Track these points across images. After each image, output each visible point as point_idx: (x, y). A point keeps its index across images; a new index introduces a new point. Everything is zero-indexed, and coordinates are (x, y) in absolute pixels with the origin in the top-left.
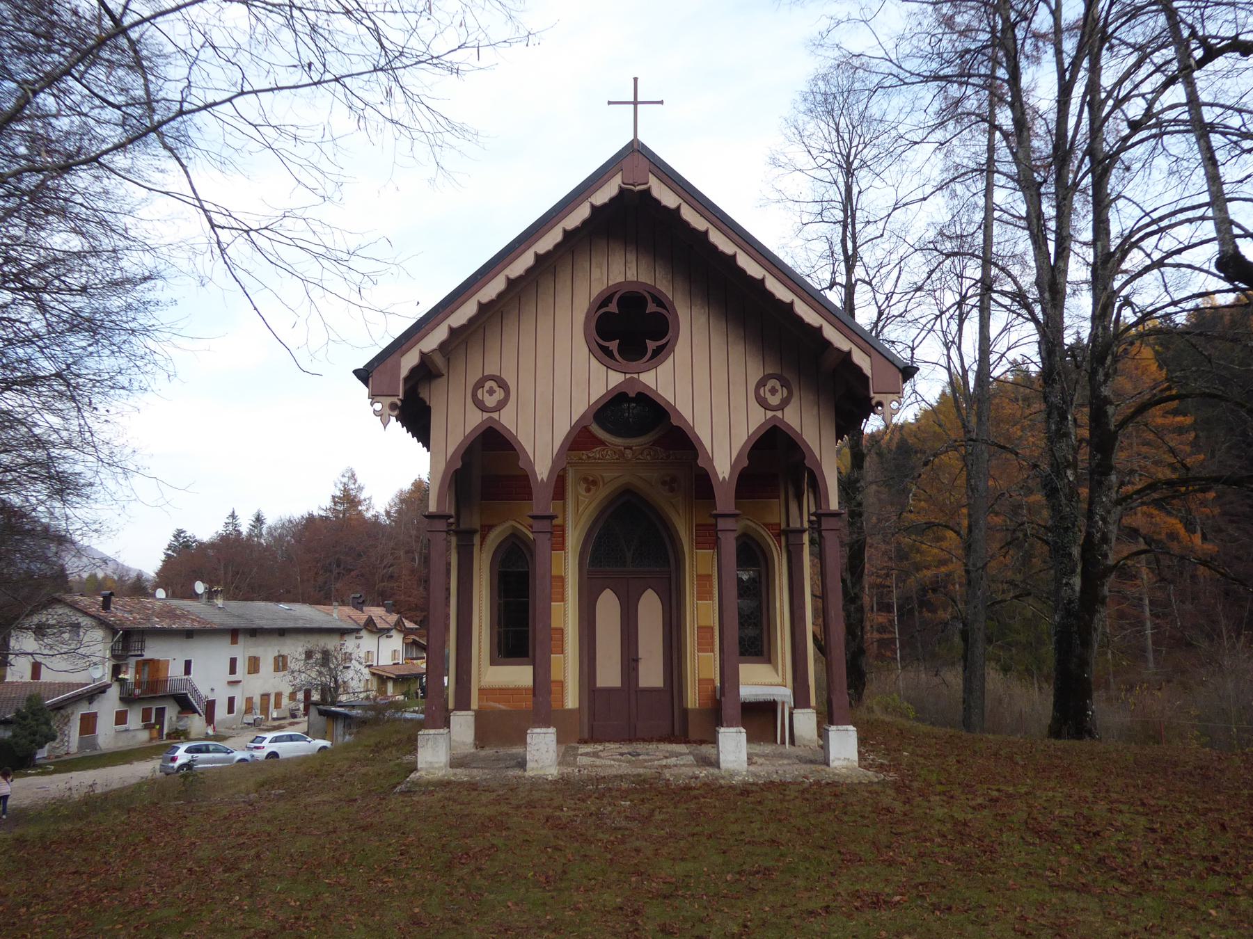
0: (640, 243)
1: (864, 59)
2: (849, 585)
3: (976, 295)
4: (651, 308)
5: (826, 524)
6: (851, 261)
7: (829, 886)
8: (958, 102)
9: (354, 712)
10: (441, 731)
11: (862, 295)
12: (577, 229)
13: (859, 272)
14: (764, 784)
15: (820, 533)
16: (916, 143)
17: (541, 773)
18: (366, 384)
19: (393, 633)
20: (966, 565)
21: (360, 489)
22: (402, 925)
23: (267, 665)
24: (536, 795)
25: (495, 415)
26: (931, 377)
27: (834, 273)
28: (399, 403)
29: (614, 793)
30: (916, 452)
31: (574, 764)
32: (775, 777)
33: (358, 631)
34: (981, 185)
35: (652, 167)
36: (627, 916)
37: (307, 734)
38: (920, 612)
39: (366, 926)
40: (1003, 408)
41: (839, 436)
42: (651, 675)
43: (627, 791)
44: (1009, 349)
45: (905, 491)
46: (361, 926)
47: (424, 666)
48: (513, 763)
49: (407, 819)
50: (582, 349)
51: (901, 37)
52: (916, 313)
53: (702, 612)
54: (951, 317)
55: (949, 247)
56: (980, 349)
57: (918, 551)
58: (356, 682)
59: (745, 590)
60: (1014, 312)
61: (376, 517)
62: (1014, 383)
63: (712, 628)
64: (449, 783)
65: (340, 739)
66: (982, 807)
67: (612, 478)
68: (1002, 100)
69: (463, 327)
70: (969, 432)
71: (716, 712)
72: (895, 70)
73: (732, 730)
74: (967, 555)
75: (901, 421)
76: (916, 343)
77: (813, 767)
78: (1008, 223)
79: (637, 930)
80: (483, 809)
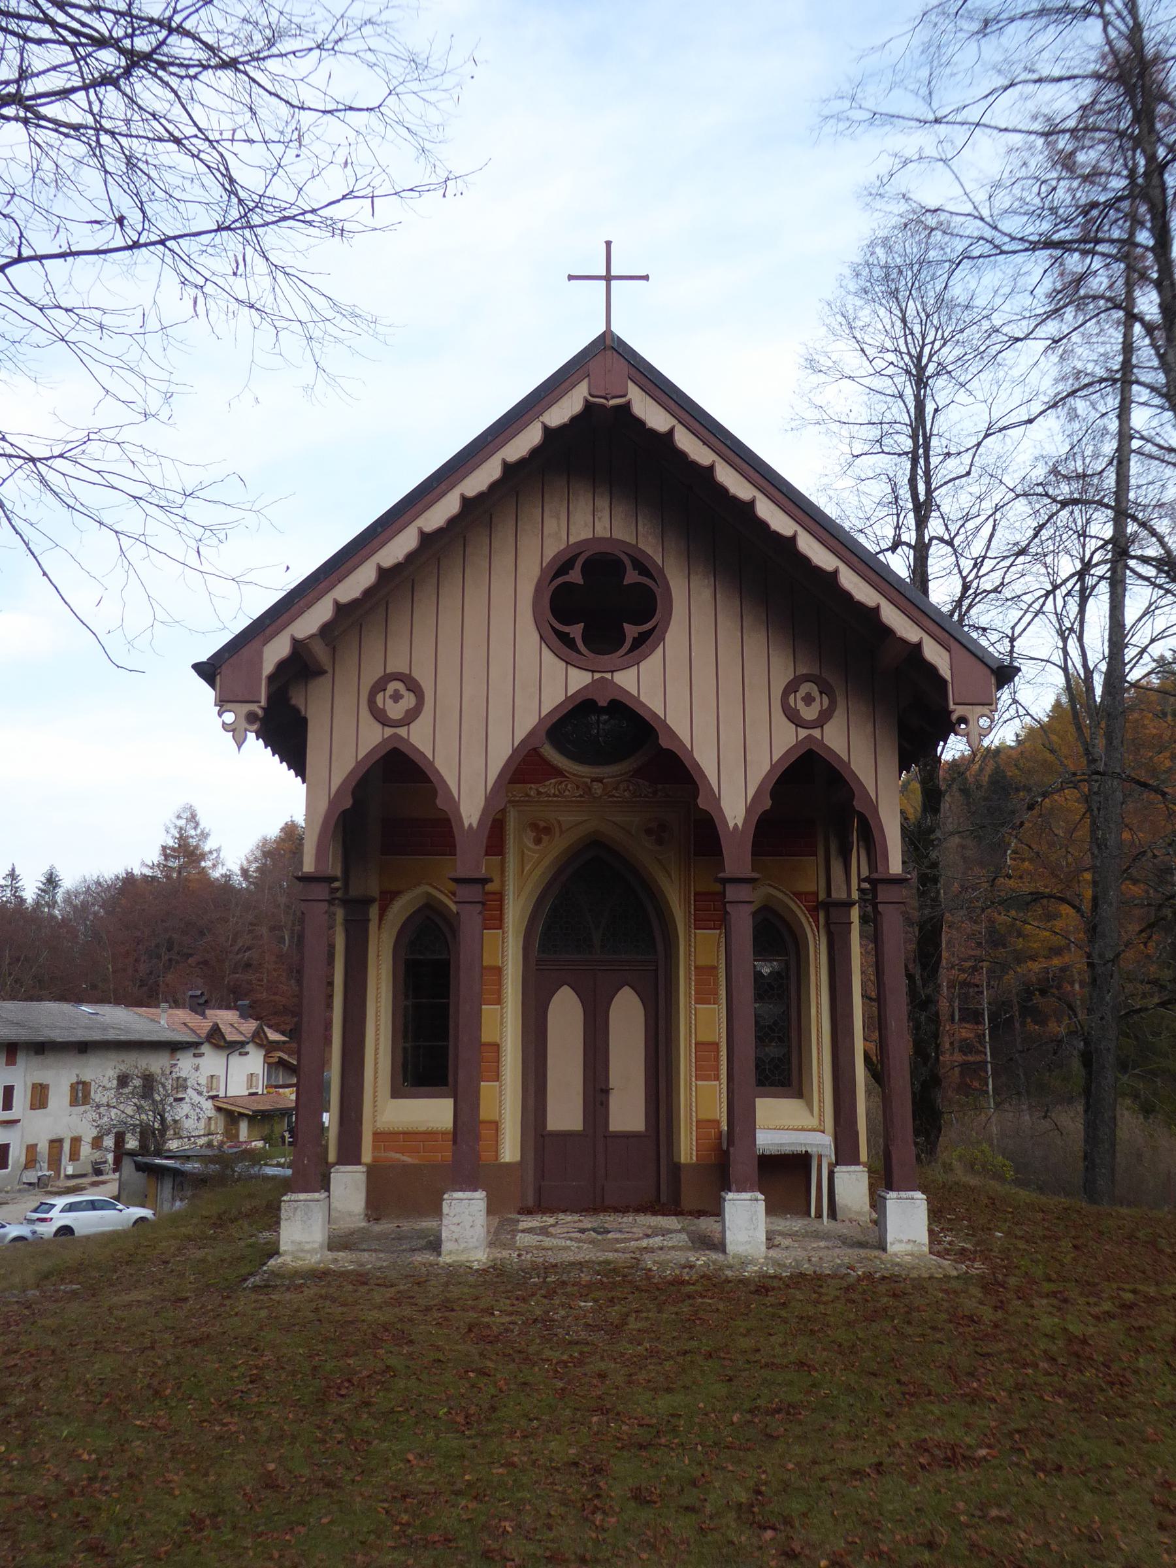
0: (611, 482)
1: (943, 217)
2: (919, 983)
3: (1104, 562)
4: (631, 577)
5: (884, 893)
6: (923, 510)
7: (882, 1431)
8: (1080, 280)
9: (189, 1166)
10: (316, 1195)
11: (939, 560)
12: (522, 462)
13: (935, 527)
14: (791, 1277)
15: (875, 906)
16: (1018, 340)
17: (463, 1258)
18: (212, 683)
19: (250, 1048)
20: (1089, 956)
21: (204, 836)
22: (248, 1489)
23: (59, 1097)
24: (455, 1292)
25: (402, 732)
26: (1039, 680)
27: (898, 527)
28: (260, 712)
29: (569, 1289)
30: (1017, 790)
31: (511, 1245)
32: (806, 1268)
33: (197, 1045)
34: (1113, 402)
35: (633, 371)
36: (584, 1475)
37: (117, 1198)
38: (1023, 1024)
39: (195, 1490)
40: (1144, 726)
41: (904, 766)
42: (627, 1113)
43: (589, 1286)
44: (1153, 641)
45: (1002, 846)
46: (188, 1491)
47: (293, 1097)
48: (423, 1242)
49: (261, 1329)
50: (530, 636)
51: (997, 185)
52: (1018, 588)
53: (703, 1021)
54: (1069, 594)
55: (1066, 490)
56: (1110, 640)
57: (1020, 935)
58: (193, 1121)
59: (765, 989)
60: (1160, 587)
61: (227, 877)
62: (1161, 691)
63: (717, 1044)
64: (326, 1273)
65: (166, 1207)
66: (1110, 1315)
67: (574, 824)
68: (1144, 277)
69: (355, 603)
70: (1094, 761)
71: (724, 1166)
72: (988, 233)
73: (747, 1195)
74: (1091, 941)
75: (996, 743)
76: (1018, 630)
77: (863, 1252)
78: (1151, 456)
79: (598, 1496)
80: (375, 1314)
